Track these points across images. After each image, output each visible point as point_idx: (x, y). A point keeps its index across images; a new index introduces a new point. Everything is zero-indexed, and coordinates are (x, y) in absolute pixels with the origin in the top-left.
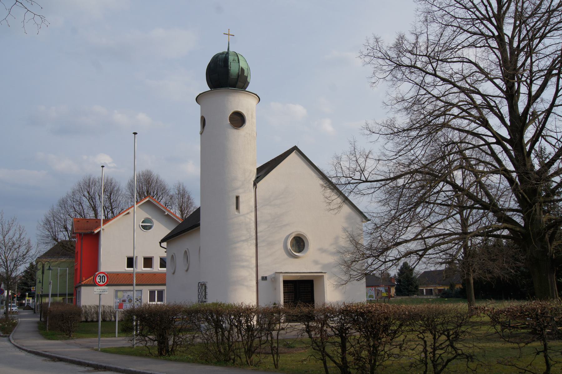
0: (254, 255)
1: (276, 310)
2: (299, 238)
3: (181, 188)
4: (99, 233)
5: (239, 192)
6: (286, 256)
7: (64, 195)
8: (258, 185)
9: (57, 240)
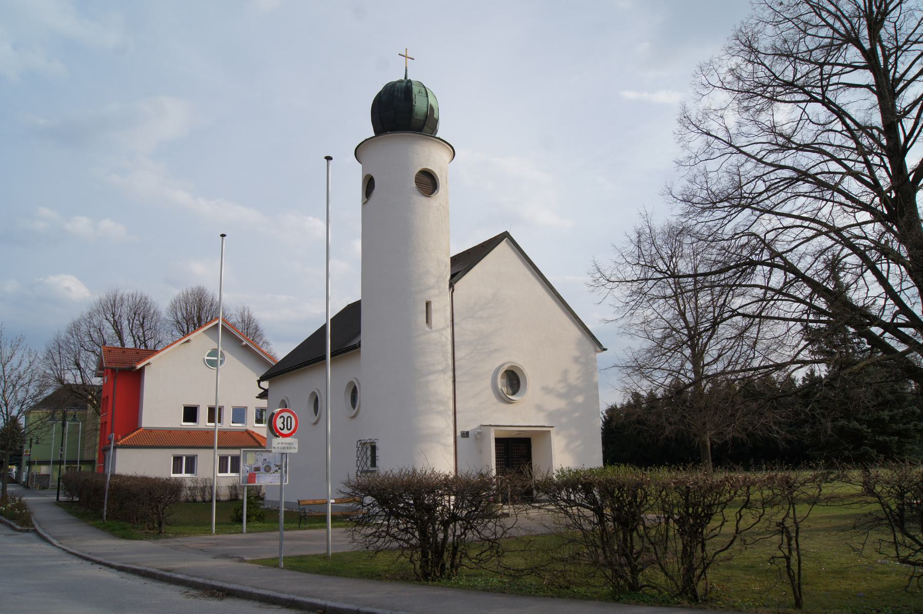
0: (451, 395)
1: (483, 482)
2: (512, 372)
3: (246, 314)
4: (142, 370)
5: (432, 295)
6: (495, 400)
7: (77, 317)
8: (456, 286)
9: (62, 383)
